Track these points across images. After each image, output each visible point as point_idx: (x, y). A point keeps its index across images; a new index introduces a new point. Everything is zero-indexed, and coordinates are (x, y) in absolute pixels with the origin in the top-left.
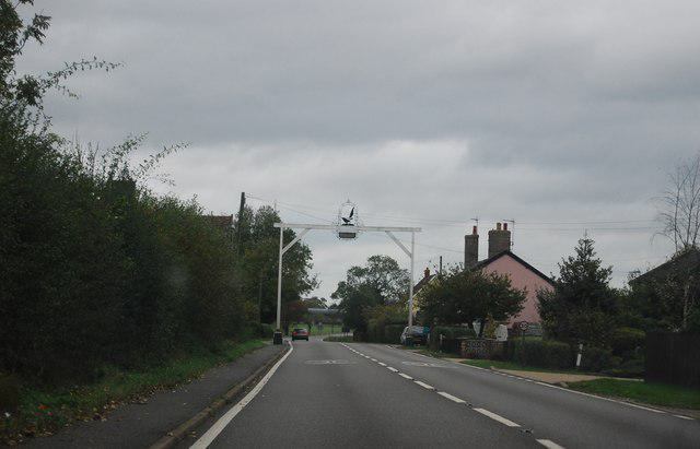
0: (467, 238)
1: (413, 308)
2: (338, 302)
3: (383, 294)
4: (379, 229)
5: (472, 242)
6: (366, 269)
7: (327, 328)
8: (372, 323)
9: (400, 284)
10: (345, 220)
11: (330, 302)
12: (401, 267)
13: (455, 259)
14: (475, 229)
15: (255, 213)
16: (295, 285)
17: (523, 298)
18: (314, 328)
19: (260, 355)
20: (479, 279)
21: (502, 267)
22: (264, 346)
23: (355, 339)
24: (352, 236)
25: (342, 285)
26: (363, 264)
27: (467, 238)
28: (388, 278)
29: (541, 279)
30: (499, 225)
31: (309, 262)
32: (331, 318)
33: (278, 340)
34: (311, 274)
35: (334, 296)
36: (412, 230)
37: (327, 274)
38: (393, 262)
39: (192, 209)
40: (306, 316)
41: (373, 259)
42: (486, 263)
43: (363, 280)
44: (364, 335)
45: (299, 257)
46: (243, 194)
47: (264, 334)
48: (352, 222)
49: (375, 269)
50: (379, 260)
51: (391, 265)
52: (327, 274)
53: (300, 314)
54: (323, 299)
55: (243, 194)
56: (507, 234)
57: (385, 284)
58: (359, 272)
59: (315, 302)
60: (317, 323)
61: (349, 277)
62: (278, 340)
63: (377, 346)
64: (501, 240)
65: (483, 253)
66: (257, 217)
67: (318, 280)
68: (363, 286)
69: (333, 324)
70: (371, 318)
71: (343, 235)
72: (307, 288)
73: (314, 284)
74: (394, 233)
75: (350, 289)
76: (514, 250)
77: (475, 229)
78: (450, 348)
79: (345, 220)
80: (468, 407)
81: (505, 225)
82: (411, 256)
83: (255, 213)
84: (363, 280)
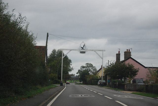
0: (117, 54)
1: (101, 74)
2: (78, 75)
3: (89, 72)
4: (92, 50)
5: (118, 56)
6: (85, 67)
8: (88, 79)
9: (94, 70)
10: (82, 48)
11: (76, 75)
12: (94, 66)
13: (113, 60)
14: (119, 51)
15: (57, 51)
16: (67, 69)
17: (138, 71)
18: (72, 81)
19: (52, 91)
20: (124, 65)
21: (129, 62)
22: (56, 86)
23: (83, 84)
24: (84, 52)
25: (79, 70)
26: (85, 65)
27: (117, 54)
29: (144, 67)
30: (127, 50)
31: (71, 63)
32: (76, 78)
33: (62, 85)
34: (71, 66)
35: (77, 73)
36: (102, 51)
37: (75, 71)
38: (92, 65)
39: (15, 24)
40: (70, 78)
42: (124, 61)
43: (84, 69)
44: (86, 83)
45: (67, 61)
46: (48, 33)
47: (57, 82)
49: (87, 66)
50: (88, 64)
51: (91, 65)
52: (75, 71)
53: (68, 77)
55: (48, 33)
56: (130, 53)
57: (90, 70)
58: (83, 67)
59: (72, 75)
60: (73, 80)
61: (81, 68)
62: (62, 85)
64: (128, 54)
65: (122, 58)
66: (57, 52)
68: (84, 71)
70: (87, 78)
71: (81, 52)
72: (70, 70)
73: (72, 69)
74: (98, 52)
75: (81, 71)
77: (119, 51)
78: (121, 87)
79: (82, 48)
81: (129, 50)
83: (57, 51)
84: (84, 69)
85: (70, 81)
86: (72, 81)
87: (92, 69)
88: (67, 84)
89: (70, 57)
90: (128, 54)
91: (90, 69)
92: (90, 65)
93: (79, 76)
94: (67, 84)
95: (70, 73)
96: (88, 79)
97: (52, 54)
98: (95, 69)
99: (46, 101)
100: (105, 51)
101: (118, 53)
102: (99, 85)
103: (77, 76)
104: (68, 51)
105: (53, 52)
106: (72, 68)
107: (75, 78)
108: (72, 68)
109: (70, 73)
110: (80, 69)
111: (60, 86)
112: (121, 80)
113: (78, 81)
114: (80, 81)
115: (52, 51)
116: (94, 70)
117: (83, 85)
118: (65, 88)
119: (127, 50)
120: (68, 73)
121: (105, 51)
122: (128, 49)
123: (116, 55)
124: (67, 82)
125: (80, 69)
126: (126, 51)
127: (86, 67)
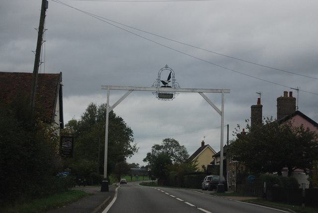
2: (146, 164)
5: (257, 110)
7: (141, 178)
9: (180, 153)
10: (163, 82)
12: (181, 145)
14: (259, 99)
15: (98, 108)
18: (134, 178)
20: (288, 130)
25: (149, 154)
26: (160, 143)
27: (253, 107)
28: (174, 151)
30: (286, 93)
32: (143, 172)
34: (132, 144)
35: (145, 160)
37: (138, 159)
38: (176, 142)
41: (166, 140)
48: (170, 84)
49: (167, 146)
50: (169, 141)
51: (175, 144)
52: (138, 159)
54: (138, 164)
56: (293, 100)
57: (172, 154)
58: (158, 147)
59: (134, 165)
60: (135, 175)
62: (105, 188)
63: (177, 189)
67: (137, 146)
69: (144, 176)
71: (163, 96)
72: (130, 153)
73: (135, 149)
75: (154, 157)
76: (301, 108)
77: (259, 99)
79: (163, 82)
80: (196, 208)
81: (291, 93)
82: (221, 113)
83: (98, 108)
85: (129, 178)
86: (134, 178)
87: (177, 153)
88: (123, 183)
89: (129, 122)
90: (287, 104)
91: (172, 152)
92: (172, 142)
93: (147, 167)
94: (123, 183)
95: (129, 160)
96: (172, 173)
97: (87, 115)
98: (183, 152)
99: (107, 200)
100: (228, 91)
101: (256, 104)
102: (206, 189)
103: (143, 167)
104: (127, 91)
105: (89, 110)
106: (134, 147)
107: (140, 171)
108: (134, 147)
109: (129, 160)
110: (151, 152)
111: (101, 191)
112: (280, 174)
113: (145, 178)
114: (153, 179)
115: (86, 107)
116: (180, 153)
117: (161, 188)
118: (115, 199)
119: (286, 93)
120: (125, 159)
121: (228, 91)
122: (289, 90)
123: (252, 110)
124: (122, 179)
125: (151, 152)
126: (283, 96)
127: (164, 148)
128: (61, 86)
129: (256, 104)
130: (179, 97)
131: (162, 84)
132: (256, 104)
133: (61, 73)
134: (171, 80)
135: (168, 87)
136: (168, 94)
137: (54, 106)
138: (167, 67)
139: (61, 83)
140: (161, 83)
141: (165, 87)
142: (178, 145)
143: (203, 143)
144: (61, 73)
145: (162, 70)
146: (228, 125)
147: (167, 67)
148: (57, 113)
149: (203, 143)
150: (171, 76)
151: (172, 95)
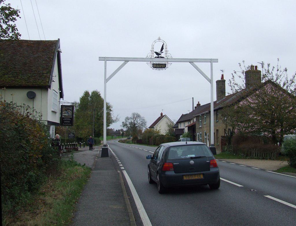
10: (157, 53)
14: (223, 75)
48: (163, 55)
51: (138, 116)
71: (157, 66)
77: (223, 75)
79: (157, 53)
81: (256, 67)
83: (90, 94)
115: (83, 92)
119: (252, 66)
128: (59, 53)
129: (220, 79)
130: (170, 66)
131: (156, 55)
132: (220, 79)
133: (59, 39)
134: (163, 51)
135: (161, 57)
136: (162, 64)
137: (50, 72)
138: (159, 39)
139: (59, 50)
140: (155, 54)
141: (158, 57)
142: (140, 116)
143: (162, 114)
144: (59, 39)
145: (155, 42)
146: (193, 98)
147: (159, 39)
148: (55, 78)
149: (162, 114)
150: (164, 47)
151: (165, 65)
